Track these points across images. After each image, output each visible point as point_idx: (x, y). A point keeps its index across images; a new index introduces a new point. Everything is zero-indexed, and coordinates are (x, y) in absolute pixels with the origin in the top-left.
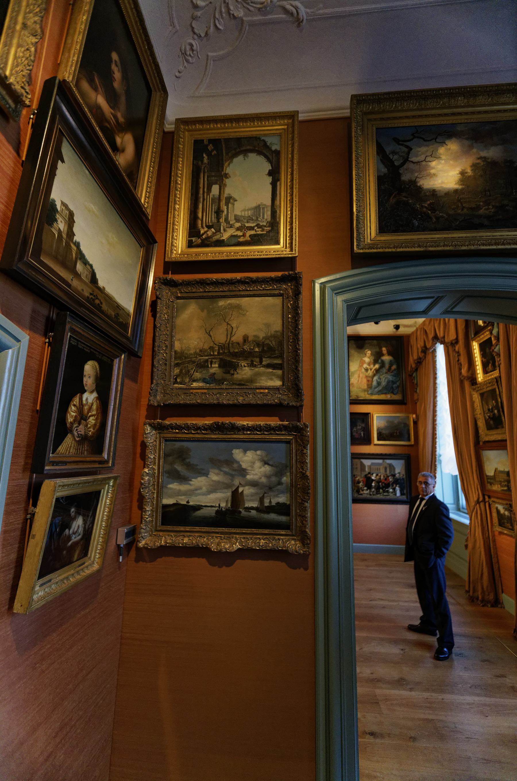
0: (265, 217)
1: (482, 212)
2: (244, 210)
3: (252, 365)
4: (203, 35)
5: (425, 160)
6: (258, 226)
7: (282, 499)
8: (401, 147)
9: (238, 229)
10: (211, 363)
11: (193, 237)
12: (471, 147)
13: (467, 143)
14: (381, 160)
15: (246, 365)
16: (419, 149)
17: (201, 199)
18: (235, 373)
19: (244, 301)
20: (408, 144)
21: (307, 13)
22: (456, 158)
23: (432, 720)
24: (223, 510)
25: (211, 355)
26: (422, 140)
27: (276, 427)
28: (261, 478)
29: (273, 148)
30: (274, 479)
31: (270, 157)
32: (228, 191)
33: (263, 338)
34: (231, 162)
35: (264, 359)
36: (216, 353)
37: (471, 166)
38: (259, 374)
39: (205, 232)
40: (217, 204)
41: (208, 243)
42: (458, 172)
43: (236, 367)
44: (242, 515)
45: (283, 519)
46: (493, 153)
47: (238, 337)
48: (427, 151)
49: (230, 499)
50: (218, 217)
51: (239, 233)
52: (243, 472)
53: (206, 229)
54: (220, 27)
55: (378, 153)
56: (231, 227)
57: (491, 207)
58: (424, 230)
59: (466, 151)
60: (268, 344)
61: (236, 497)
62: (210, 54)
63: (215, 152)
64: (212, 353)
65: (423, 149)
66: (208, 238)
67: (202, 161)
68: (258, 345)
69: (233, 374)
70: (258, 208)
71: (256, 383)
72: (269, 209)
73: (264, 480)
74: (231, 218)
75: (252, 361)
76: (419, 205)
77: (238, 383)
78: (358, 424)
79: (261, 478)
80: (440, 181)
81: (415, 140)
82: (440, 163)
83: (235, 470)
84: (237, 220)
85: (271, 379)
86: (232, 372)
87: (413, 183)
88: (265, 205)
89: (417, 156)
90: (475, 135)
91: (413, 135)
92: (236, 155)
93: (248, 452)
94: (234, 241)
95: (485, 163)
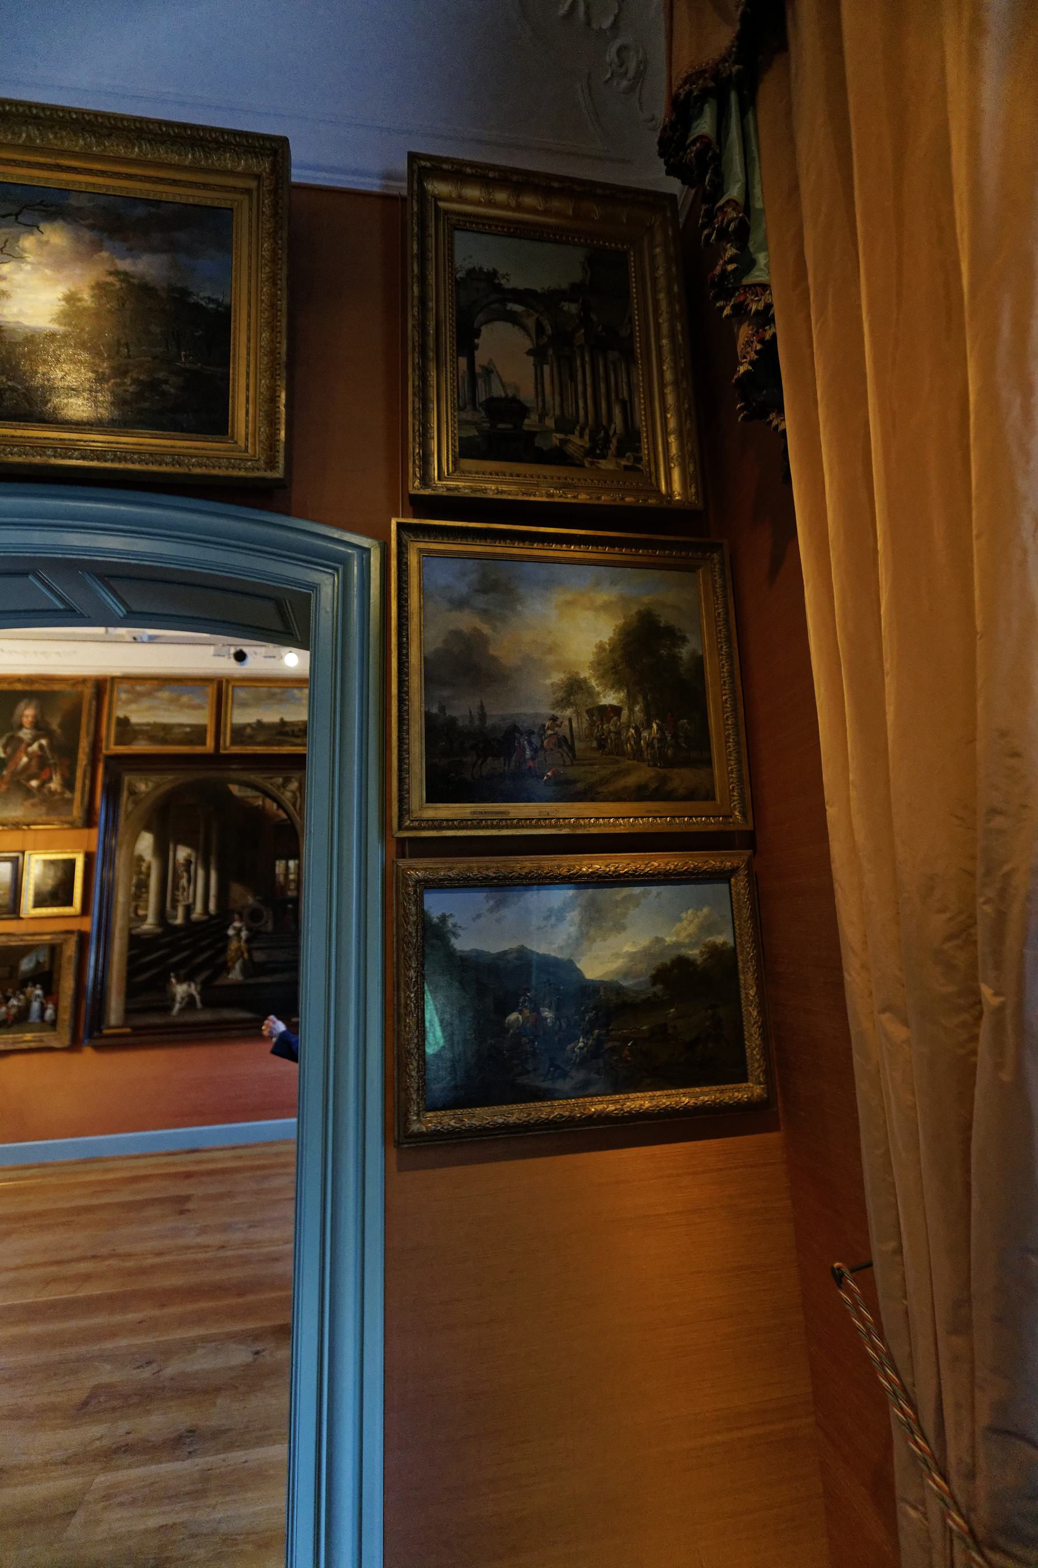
12: (97, 246)
13: (88, 235)
22: (58, 263)
42: (60, 296)
57: (128, 381)
59: (87, 252)
82: (22, 270)
90: (108, 223)
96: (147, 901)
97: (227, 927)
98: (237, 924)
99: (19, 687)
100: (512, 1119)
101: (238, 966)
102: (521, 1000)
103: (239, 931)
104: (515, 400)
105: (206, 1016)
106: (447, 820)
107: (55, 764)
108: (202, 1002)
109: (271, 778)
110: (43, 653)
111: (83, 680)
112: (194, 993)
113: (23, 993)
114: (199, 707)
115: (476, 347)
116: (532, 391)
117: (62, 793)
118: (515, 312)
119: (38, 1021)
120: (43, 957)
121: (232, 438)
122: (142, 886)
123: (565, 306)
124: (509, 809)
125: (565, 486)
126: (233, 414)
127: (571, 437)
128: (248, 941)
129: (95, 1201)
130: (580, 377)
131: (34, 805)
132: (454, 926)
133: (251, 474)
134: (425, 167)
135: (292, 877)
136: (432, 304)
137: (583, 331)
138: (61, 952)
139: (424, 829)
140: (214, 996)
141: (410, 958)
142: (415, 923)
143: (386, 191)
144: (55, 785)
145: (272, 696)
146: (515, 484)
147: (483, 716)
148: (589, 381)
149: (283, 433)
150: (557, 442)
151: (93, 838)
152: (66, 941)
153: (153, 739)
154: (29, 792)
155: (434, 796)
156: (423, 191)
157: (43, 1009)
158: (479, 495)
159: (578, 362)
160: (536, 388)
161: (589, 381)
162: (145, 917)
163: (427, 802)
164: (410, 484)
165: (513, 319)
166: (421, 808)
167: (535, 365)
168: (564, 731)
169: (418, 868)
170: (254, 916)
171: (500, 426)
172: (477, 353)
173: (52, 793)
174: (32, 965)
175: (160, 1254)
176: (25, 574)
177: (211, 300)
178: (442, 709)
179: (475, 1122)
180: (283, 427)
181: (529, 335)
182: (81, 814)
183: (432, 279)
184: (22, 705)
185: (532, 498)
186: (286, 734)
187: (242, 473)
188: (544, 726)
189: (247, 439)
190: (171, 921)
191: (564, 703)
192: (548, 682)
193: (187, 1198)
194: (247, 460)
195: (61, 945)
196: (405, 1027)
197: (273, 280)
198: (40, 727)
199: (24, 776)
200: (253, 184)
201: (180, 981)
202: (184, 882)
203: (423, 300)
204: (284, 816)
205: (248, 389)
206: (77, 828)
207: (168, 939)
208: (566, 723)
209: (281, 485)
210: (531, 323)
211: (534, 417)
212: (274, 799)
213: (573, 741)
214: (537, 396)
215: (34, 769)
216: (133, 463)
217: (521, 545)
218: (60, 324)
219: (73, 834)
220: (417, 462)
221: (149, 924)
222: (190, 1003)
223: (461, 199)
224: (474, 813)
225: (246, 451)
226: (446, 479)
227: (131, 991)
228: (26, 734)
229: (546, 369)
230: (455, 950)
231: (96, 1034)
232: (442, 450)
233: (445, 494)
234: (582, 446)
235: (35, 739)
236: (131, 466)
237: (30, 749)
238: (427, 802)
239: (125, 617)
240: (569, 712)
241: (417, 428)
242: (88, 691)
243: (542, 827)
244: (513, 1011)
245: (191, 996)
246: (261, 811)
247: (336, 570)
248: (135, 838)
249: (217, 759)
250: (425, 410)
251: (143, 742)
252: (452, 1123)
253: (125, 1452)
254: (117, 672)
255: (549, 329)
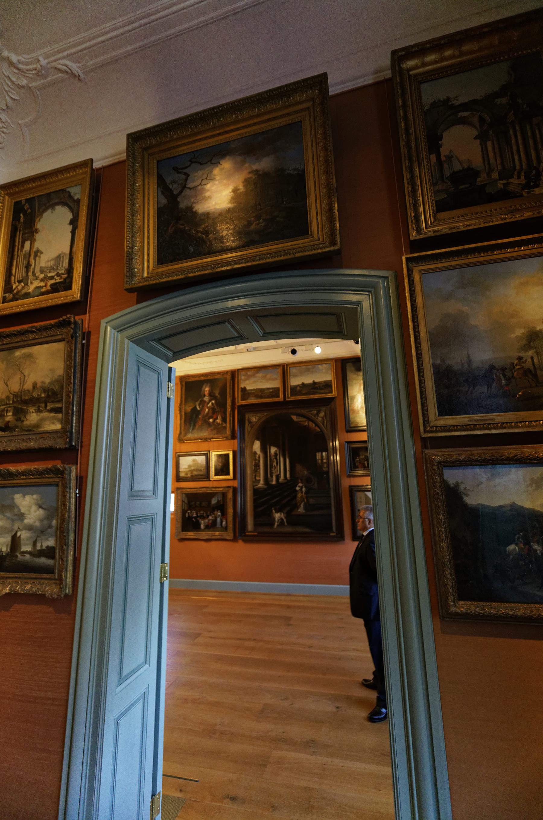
0: (64, 265)
1: (253, 227)
2: (48, 261)
3: (39, 411)
4: (5, 108)
5: (201, 184)
6: (58, 275)
7: (51, 542)
8: (180, 175)
9: (42, 280)
10: (7, 411)
11: (7, 293)
12: (243, 162)
13: (239, 159)
14: (162, 192)
15: (34, 411)
16: (196, 174)
17: (16, 257)
18: (25, 419)
19: (36, 349)
20: (185, 171)
21: (79, 67)
22: (229, 176)
23: (313, 789)
24: (4, 554)
25: (7, 404)
26: (199, 164)
27: (44, 470)
28: (35, 522)
29: (76, 198)
30: (46, 522)
31: (73, 206)
32: (38, 245)
33: (49, 383)
34: (42, 217)
35: (48, 404)
36: (11, 402)
37: (243, 182)
38: (43, 419)
39: (17, 287)
40: (27, 259)
41: (18, 297)
42: (230, 190)
43: (25, 413)
44: (18, 559)
45: (50, 562)
46: (265, 164)
47: (28, 386)
48: (203, 174)
49: (10, 543)
50: (27, 272)
51: (43, 284)
52: (21, 516)
53: (17, 284)
54: (16, 98)
55: (158, 185)
56: (37, 279)
57: (261, 221)
58: (198, 256)
59: (238, 167)
60: (52, 389)
61: (15, 542)
62: (20, 122)
63: (30, 210)
64: (8, 402)
65: (200, 173)
66: (19, 292)
67: (19, 220)
68: (44, 391)
69: (23, 421)
70: (59, 258)
71: (44, 428)
72: (68, 256)
73: (38, 524)
74: (37, 270)
75: (39, 407)
76: (195, 230)
77: (26, 429)
78: (361, 453)
79: (35, 522)
80: (214, 203)
81: (193, 165)
82: (215, 184)
83: (16, 515)
84: (42, 272)
85: (53, 423)
86: (22, 419)
87: (190, 209)
88: (64, 253)
89: (193, 181)
90: (246, 150)
91: (190, 161)
92: (45, 211)
93: (26, 496)
94: (38, 292)
95: (256, 176)
96: (260, 473)
97: (296, 486)
98: (300, 485)
99: (202, 378)
100: (519, 613)
101: (302, 505)
102: (516, 537)
103: (301, 488)
104: (469, 169)
105: (289, 529)
106: (454, 426)
107: (218, 411)
108: (287, 522)
109: (311, 411)
110: (210, 362)
111: (226, 373)
112: (283, 518)
113: (214, 514)
114: (275, 379)
115: (441, 146)
116: (481, 160)
117: (222, 424)
118: (464, 117)
119: (220, 527)
120: (220, 498)
121: (311, 235)
122: (257, 466)
123: (498, 101)
124: (495, 417)
125: (513, 212)
126: (310, 223)
127: (511, 180)
128: (306, 493)
129: (249, 612)
130: (513, 141)
131: (212, 430)
132: (465, 489)
133: (324, 250)
134: (401, 55)
135: (325, 461)
136: (412, 130)
137: (512, 112)
138: (227, 496)
139: (439, 431)
140: (293, 520)
141: (439, 507)
142: (440, 487)
143: (376, 80)
144: (219, 421)
145: (308, 370)
146: (475, 219)
147: (469, 362)
148: (520, 142)
149: (338, 225)
150: (502, 186)
151: (235, 443)
152: (228, 491)
153: (257, 396)
154: (209, 424)
155: (443, 411)
156: (401, 69)
157: (222, 522)
158: (454, 231)
159: (512, 133)
160: (483, 158)
161: (520, 142)
162: (259, 481)
163: (439, 415)
164: (411, 235)
165: (463, 121)
166: (436, 419)
167: (481, 144)
168: (528, 364)
169: (438, 455)
170: (308, 481)
171: (461, 187)
172: (441, 149)
173: (218, 424)
174: (216, 501)
175: (282, 644)
176: (224, 322)
177: (295, 170)
178: (443, 361)
179: (493, 611)
180: (337, 222)
181: (475, 127)
182: (230, 433)
183: (410, 116)
184: (204, 386)
185: (491, 224)
186: (317, 388)
187: (320, 251)
188: (513, 363)
189: (318, 234)
190: (270, 483)
191: (527, 346)
192: (513, 336)
193: (290, 618)
194: (320, 244)
195: (226, 492)
196: (440, 548)
197: (325, 148)
198: (212, 395)
199: (207, 418)
200: (310, 104)
201: (277, 512)
202: (275, 464)
203: (407, 129)
204: (319, 430)
205: (317, 208)
206: (229, 439)
207: (269, 491)
208: (530, 360)
209: (338, 252)
210: (475, 120)
211: (484, 175)
212: (313, 422)
213: (536, 372)
214: (484, 162)
215: (210, 414)
216: (269, 259)
217: (486, 254)
218: (232, 203)
219: (227, 442)
220: (413, 221)
221: (261, 484)
222: (281, 522)
223: (424, 64)
224: (471, 421)
225: (319, 240)
226: (433, 225)
227: (256, 515)
228: (206, 399)
229: (489, 144)
230: (467, 504)
231: (243, 534)
232: (426, 212)
233: (433, 235)
234: (519, 184)
235: (210, 401)
236: (268, 261)
237: (209, 405)
238: (439, 415)
239: (263, 336)
240: (530, 353)
241: (411, 202)
242: (229, 377)
243: (519, 427)
244: (512, 544)
245: (282, 519)
246: (308, 427)
247: (370, 292)
248: (252, 444)
249: (285, 403)
250: (414, 192)
251: (252, 398)
252: (477, 610)
253: (283, 741)
254: (240, 367)
255: (488, 120)
